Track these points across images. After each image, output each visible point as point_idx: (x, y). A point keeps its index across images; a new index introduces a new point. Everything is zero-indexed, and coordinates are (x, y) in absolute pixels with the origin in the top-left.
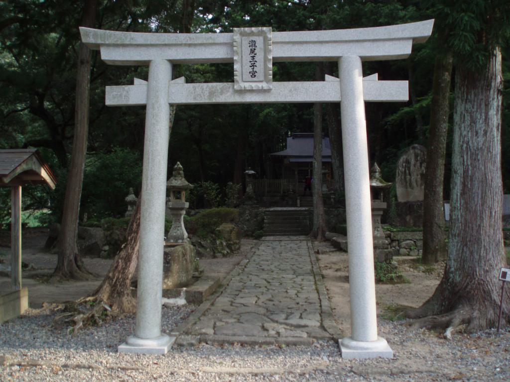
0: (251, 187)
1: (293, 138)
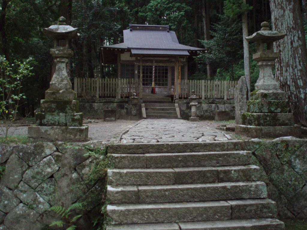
0: (65, 73)
1: (131, 30)
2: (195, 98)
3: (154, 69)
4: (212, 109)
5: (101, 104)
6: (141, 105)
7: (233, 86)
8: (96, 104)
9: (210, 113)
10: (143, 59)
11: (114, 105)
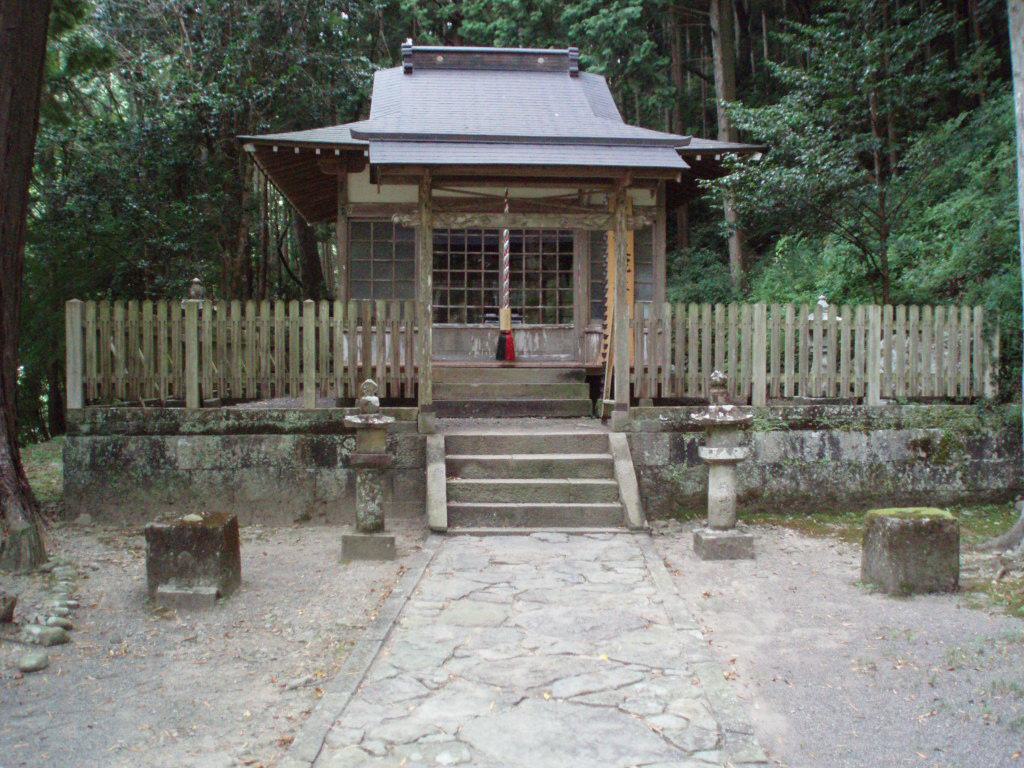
1: (408, 71)
2: (730, 418)
3: (506, 244)
4: (803, 459)
5: (213, 441)
6: (425, 440)
7: (913, 333)
8: (181, 441)
9: (793, 478)
10: (436, 193)
11: (281, 446)
